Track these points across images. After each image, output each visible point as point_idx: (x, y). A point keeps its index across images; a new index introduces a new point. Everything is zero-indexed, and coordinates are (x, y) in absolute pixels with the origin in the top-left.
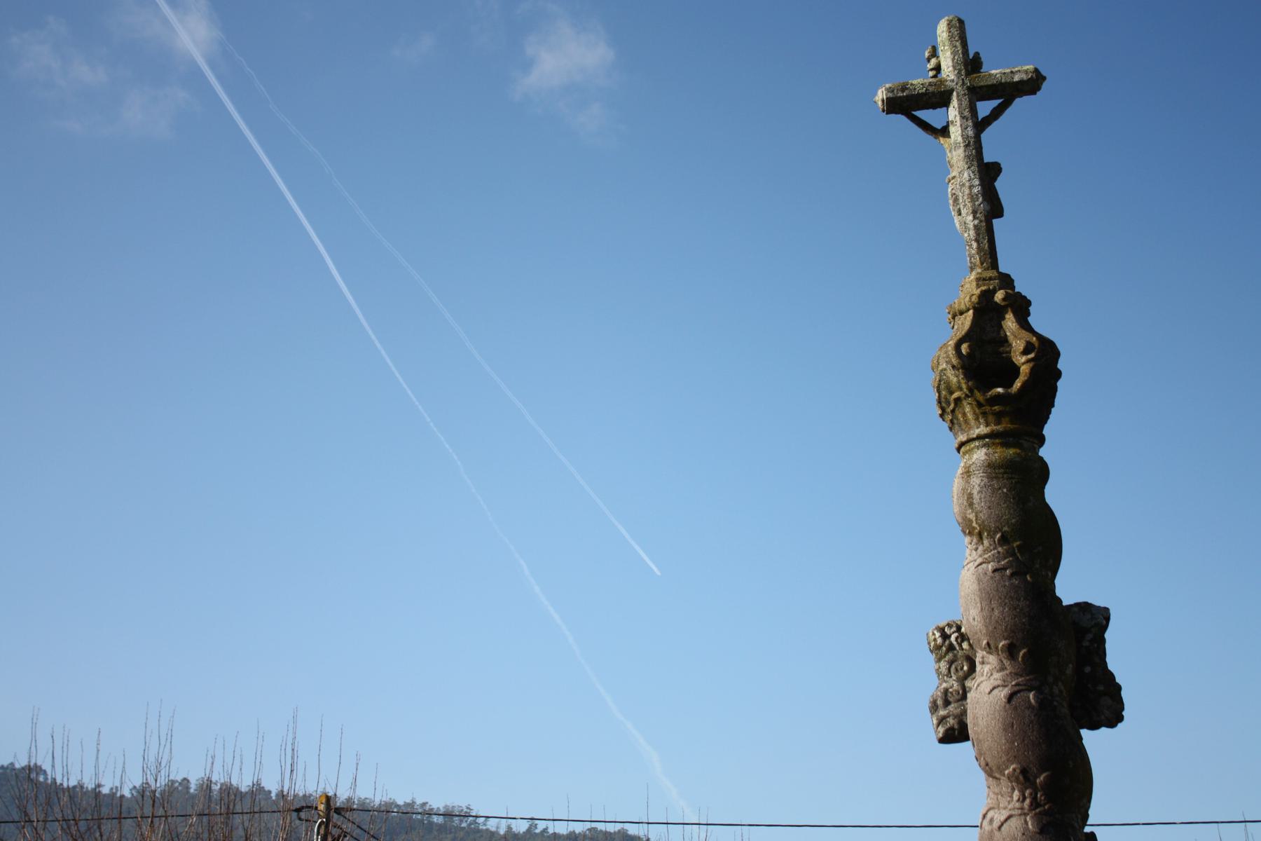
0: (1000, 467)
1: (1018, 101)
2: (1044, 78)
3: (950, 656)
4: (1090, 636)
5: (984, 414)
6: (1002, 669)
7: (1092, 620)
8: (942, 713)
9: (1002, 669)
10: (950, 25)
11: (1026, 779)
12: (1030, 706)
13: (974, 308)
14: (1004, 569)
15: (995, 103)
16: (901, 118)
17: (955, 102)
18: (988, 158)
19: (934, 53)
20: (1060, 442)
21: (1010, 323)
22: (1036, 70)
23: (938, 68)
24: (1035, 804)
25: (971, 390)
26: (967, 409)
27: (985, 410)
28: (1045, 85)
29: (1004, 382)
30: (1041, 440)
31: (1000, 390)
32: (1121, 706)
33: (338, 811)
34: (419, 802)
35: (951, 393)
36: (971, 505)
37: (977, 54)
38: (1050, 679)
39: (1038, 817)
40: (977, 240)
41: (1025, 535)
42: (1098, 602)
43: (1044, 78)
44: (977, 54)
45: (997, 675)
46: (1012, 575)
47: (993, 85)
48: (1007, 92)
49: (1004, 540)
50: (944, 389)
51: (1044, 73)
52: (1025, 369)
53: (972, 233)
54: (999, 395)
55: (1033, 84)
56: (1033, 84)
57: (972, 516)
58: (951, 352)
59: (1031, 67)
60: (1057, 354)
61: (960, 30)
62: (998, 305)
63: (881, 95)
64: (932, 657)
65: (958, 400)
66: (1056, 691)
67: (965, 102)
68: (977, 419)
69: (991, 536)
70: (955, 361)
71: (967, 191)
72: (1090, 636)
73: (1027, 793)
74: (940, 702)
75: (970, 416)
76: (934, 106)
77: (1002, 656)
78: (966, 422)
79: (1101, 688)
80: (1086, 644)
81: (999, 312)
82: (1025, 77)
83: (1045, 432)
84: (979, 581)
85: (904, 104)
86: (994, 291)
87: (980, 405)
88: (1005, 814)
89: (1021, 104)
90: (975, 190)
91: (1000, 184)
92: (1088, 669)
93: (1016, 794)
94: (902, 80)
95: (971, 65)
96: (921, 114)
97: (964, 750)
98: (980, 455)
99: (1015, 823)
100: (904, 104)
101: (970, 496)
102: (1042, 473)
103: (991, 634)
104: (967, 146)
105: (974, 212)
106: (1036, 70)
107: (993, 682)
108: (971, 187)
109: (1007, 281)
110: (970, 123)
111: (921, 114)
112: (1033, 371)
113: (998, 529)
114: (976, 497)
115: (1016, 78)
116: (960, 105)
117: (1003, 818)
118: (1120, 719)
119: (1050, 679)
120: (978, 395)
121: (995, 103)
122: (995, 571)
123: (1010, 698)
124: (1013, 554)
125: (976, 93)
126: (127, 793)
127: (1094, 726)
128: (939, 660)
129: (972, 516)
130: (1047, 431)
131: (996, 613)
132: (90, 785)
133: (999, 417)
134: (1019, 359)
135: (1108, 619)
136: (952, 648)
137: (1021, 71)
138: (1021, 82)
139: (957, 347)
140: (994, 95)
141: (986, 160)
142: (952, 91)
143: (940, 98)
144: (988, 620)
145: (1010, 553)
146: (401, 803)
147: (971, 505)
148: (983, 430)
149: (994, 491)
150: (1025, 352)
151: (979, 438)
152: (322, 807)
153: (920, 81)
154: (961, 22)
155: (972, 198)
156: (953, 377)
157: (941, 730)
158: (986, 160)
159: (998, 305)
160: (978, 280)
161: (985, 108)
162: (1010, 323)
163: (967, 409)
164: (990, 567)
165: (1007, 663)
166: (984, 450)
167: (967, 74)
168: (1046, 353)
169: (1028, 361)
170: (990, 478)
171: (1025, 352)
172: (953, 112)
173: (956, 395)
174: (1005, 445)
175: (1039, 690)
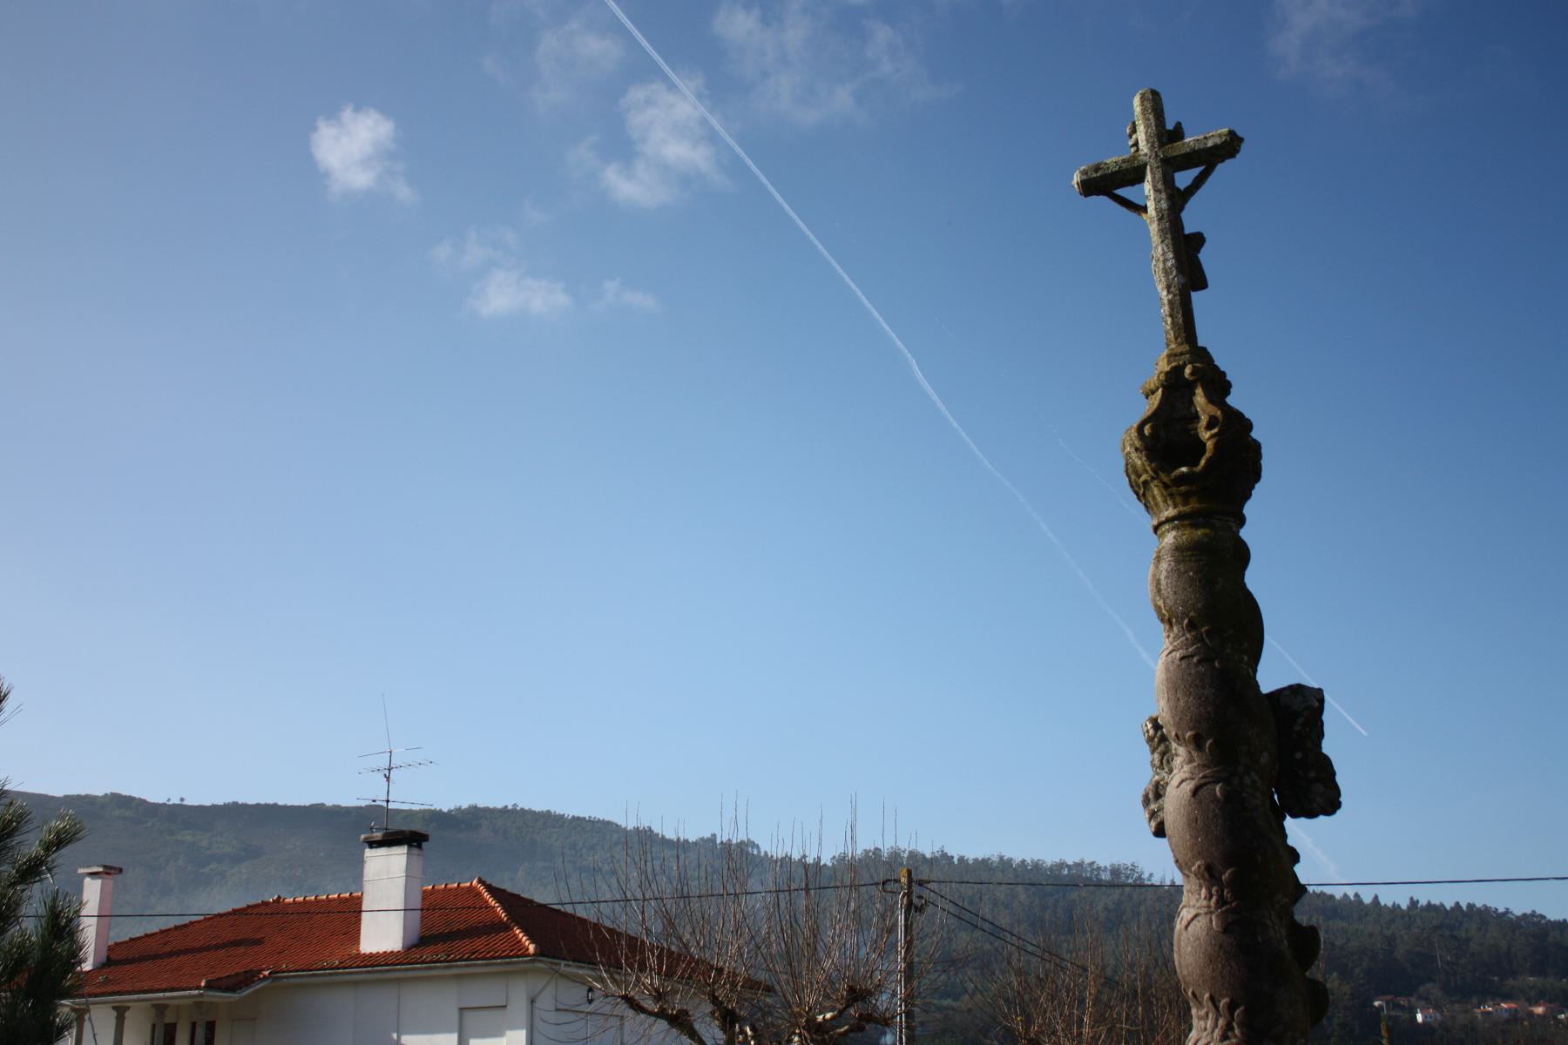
0: (1187, 549)
1: (1220, 167)
2: (1241, 140)
3: (1162, 747)
4: (1301, 720)
5: (1172, 495)
6: (1191, 761)
7: (1302, 708)
8: (1153, 806)
9: (1191, 761)
10: (1143, 98)
11: (1212, 876)
12: (1216, 799)
13: (1163, 386)
14: (1192, 656)
15: (1194, 173)
16: (1103, 201)
17: (1149, 177)
18: (1189, 229)
19: (1134, 131)
20: (1263, 521)
21: (1200, 398)
22: (1232, 133)
23: (1136, 144)
24: (1221, 902)
25: (1155, 471)
26: (1156, 492)
27: (1172, 489)
28: (1243, 146)
29: (1199, 460)
30: (1241, 521)
31: (1184, 469)
32: (1336, 791)
33: (921, 883)
34: (1087, 861)
35: (1139, 476)
36: (1159, 591)
37: (1179, 126)
38: (1241, 769)
39: (1222, 917)
40: (1171, 316)
41: (1217, 614)
42: (1313, 683)
43: (1241, 140)
44: (1179, 126)
45: (1186, 768)
46: (1199, 662)
47: (1186, 154)
48: (1210, 158)
49: (1192, 626)
50: (1131, 471)
51: (1240, 134)
52: (1210, 445)
53: (1167, 307)
54: (1183, 474)
55: (1230, 146)
56: (1230, 146)
57: (1160, 603)
58: (1134, 434)
59: (1225, 130)
60: (1248, 425)
61: (1155, 103)
62: (1193, 377)
63: (1076, 178)
64: (1147, 748)
65: (1145, 483)
66: (1247, 780)
67: (1159, 175)
68: (1165, 501)
69: (1179, 623)
70: (1138, 443)
71: (1161, 265)
72: (1301, 720)
73: (1214, 890)
74: (1151, 796)
75: (1159, 499)
76: (1132, 184)
77: (1191, 747)
78: (1157, 504)
79: (1312, 774)
80: (1297, 728)
81: (1189, 388)
82: (1218, 141)
83: (1246, 511)
84: (1167, 670)
85: (1102, 184)
86: (1184, 366)
87: (1166, 486)
88: (1193, 912)
89: (1223, 169)
90: (1169, 264)
91: (1204, 256)
92: (1298, 755)
93: (1204, 891)
94: (1094, 161)
95: (1166, 136)
96: (1119, 192)
97: (1164, 841)
98: (1170, 538)
99: (1202, 922)
100: (1102, 184)
101: (1158, 583)
102: (1241, 556)
103: (1177, 725)
104: (1160, 220)
105: (1168, 287)
106: (1232, 133)
107: (1183, 775)
108: (1165, 261)
109: (1202, 355)
110: (1164, 196)
111: (1119, 192)
112: (1216, 446)
113: (1185, 614)
114: (1163, 582)
115: (1210, 144)
116: (1153, 178)
117: (1190, 917)
118: (1338, 805)
119: (1241, 769)
120: (1162, 475)
121: (1194, 173)
122: (1182, 659)
123: (1195, 792)
124: (1201, 640)
125: (1171, 165)
126: (826, 860)
127: (1294, 816)
128: (1153, 752)
129: (1160, 603)
130: (1248, 509)
131: (1182, 703)
132: (796, 856)
133: (1186, 498)
134: (1205, 435)
135: (1322, 701)
136: (1158, 738)
137: (1215, 134)
138: (1215, 147)
139: (1140, 429)
140: (1187, 161)
141: (1187, 231)
142: (1145, 165)
143: (1135, 175)
144: (1174, 709)
145: (1198, 639)
146: (1070, 862)
147: (1159, 591)
148: (1171, 512)
149: (1180, 575)
150: (1209, 427)
151: (1168, 520)
152: (904, 880)
153: (1113, 160)
154: (1155, 93)
155: (1166, 272)
156: (1139, 461)
157: (1153, 824)
158: (1187, 231)
159: (1193, 377)
160: (1169, 356)
161: (1183, 179)
162: (1200, 398)
163: (1156, 492)
164: (1178, 655)
165: (1195, 754)
166: (1174, 533)
167: (1161, 146)
168: (1236, 428)
169: (1212, 437)
170: (1178, 562)
171: (1209, 427)
172: (1147, 187)
173: (1143, 478)
174: (1195, 526)
175: (1226, 781)
